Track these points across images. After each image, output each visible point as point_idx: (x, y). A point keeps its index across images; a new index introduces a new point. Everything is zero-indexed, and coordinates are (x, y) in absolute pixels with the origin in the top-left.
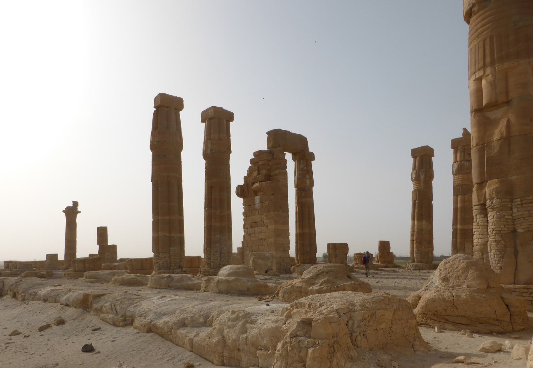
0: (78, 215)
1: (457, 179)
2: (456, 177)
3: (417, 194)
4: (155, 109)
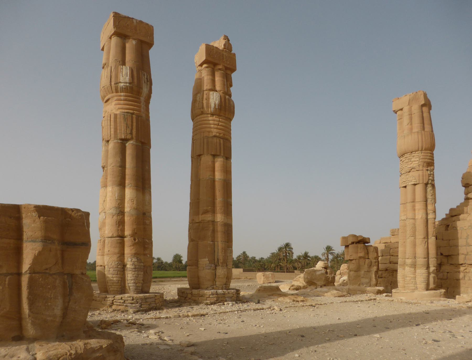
3: (132, 122)
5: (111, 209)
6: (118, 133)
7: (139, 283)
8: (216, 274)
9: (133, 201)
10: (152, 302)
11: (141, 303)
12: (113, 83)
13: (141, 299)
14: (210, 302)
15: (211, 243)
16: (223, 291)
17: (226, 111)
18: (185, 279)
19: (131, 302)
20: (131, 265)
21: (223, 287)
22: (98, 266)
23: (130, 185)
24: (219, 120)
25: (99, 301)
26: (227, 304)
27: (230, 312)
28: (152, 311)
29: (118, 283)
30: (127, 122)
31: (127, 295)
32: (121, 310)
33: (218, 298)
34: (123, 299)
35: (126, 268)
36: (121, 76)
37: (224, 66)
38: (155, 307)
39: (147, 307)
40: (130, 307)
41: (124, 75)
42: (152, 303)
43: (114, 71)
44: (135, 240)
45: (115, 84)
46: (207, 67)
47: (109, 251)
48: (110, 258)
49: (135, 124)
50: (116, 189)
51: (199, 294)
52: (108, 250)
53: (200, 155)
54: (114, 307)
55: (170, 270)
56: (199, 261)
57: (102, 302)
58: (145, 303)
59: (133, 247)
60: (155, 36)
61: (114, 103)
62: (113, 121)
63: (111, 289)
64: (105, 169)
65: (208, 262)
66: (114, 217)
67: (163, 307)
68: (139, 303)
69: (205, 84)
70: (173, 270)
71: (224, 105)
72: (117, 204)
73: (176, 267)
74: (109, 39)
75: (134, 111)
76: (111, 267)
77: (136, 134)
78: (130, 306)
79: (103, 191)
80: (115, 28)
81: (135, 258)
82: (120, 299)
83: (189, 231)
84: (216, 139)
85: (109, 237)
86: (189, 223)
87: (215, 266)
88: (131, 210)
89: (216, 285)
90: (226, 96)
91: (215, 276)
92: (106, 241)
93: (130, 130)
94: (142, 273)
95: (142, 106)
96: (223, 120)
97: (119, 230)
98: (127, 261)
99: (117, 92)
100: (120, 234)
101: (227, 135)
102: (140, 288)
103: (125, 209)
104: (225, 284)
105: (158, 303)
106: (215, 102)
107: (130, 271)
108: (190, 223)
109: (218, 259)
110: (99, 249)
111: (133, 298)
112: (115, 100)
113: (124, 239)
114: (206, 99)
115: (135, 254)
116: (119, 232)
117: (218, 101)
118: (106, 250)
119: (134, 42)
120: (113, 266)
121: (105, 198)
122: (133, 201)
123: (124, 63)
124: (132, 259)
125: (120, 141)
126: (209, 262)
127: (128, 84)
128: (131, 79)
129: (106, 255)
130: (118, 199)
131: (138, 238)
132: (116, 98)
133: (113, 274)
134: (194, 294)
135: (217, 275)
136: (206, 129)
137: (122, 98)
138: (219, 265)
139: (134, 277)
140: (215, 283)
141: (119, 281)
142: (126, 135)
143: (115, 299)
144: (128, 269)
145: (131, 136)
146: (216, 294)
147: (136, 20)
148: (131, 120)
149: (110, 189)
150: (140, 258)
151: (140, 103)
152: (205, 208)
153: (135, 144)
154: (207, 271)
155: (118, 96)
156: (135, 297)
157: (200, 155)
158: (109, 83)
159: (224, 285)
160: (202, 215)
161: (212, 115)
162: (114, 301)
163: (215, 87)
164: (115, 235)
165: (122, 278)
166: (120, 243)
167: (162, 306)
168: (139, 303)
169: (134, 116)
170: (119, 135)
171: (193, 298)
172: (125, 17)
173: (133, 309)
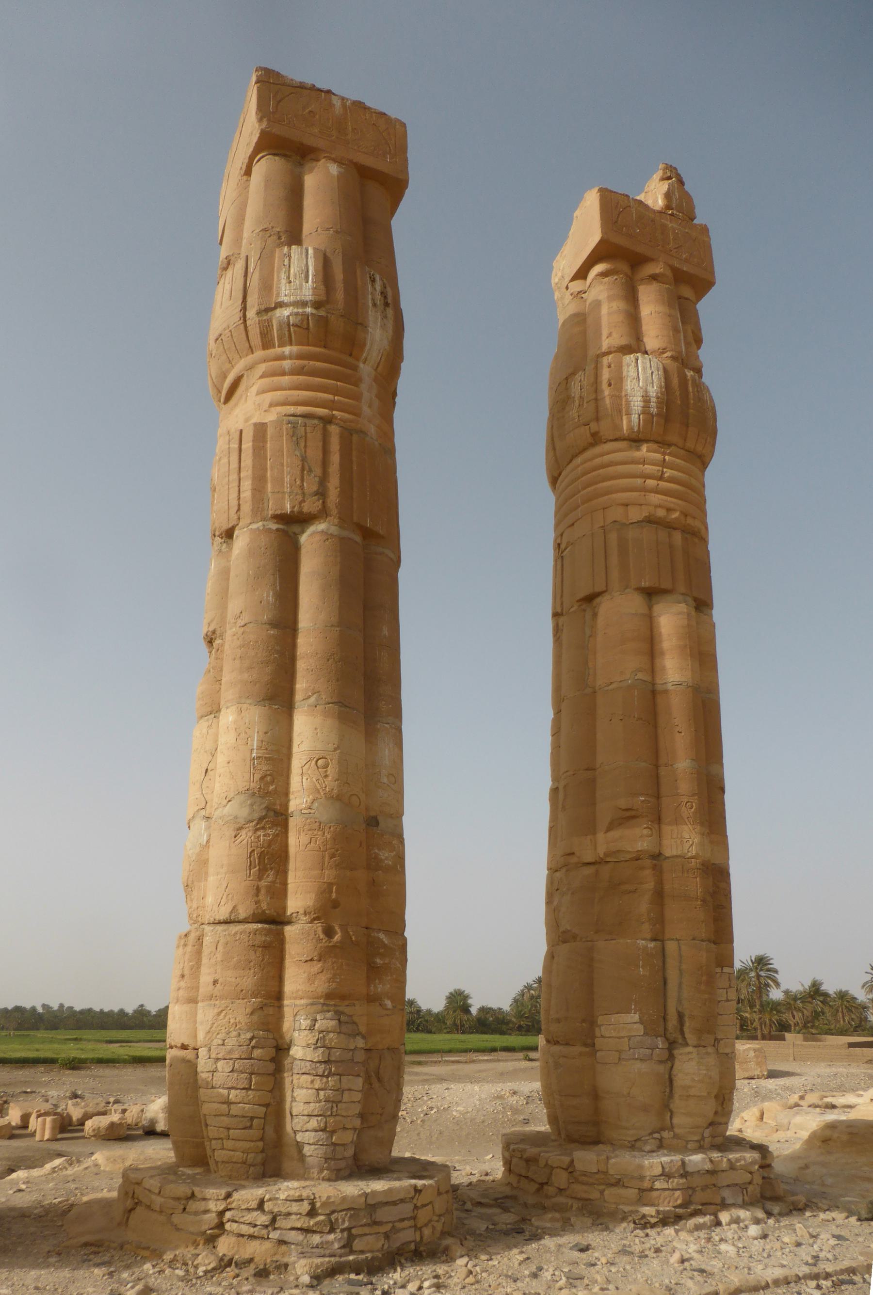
3: (326, 451)
4: (40, 1010)
5: (229, 801)
6: (270, 495)
7: (345, 1128)
8: (671, 1081)
9: (326, 766)
10: (402, 1220)
11: (349, 1229)
12: (251, 314)
13: (353, 1209)
14: (658, 1212)
15: (652, 945)
16: (711, 1161)
17: (687, 426)
18: (481, 1058)
19: (305, 1226)
20: (308, 1045)
21: (703, 1138)
22: (171, 1047)
23: (312, 700)
24: (664, 460)
25: (161, 1212)
26: (729, 1224)
27: (777, 1283)
28: (399, 1269)
29: (251, 1127)
30: (305, 451)
31: (289, 1189)
32: (256, 1260)
33: (690, 1192)
34: (267, 1206)
35: (286, 1062)
36: (284, 281)
37: (669, 266)
38: (413, 1247)
39: (380, 1245)
40: (300, 1249)
41: (295, 275)
42: (399, 1225)
43: (258, 268)
44: (329, 932)
45: (259, 313)
46: (603, 274)
47: (215, 982)
48: (219, 1014)
49: (335, 459)
50: (255, 714)
51: (606, 1173)
52: (210, 980)
53: (590, 598)
54: (225, 1246)
55: (440, 1031)
56: (599, 1023)
57: (177, 1219)
58: (366, 1230)
59: (320, 965)
60: (411, 154)
61: (254, 390)
62: (250, 451)
63: (220, 1155)
64: (217, 642)
65: (641, 1027)
66: (243, 832)
67: (449, 1241)
68: (342, 1231)
69: (605, 332)
70: (448, 1033)
71: (679, 402)
72: (257, 777)
73: (455, 1024)
74: (245, 178)
75: (332, 409)
76: (220, 1056)
77: (339, 496)
78: (297, 1244)
79: (205, 731)
80: (265, 120)
81: (329, 1015)
82: (253, 1209)
83: (549, 901)
84: (656, 528)
85: (220, 923)
86: (549, 869)
87: (667, 1045)
88: (316, 805)
89: (672, 1128)
90: (686, 370)
91: (668, 1090)
92: (207, 940)
93: (317, 479)
94: (359, 1083)
95: (366, 395)
96: (678, 461)
97: (263, 891)
98: (294, 1030)
99: (267, 344)
100: (264, 906)
101: (694, 518)
102: (350, 1152)
103: (289, 801)
104: (711, 1124)
105: (426, 1225)
106: (646, 391)
107: (305, 1076)
108: (553, 870)
109: (681, 1016)
110: (180, 973)
111: (312, 1204)
112: (261, 377)
113: (283, 929)
114: (610, 385)
115: (329, 996)
116: (261, 897)
117: (655, 388)
118: (206, 978)
119: (334, 169)
120: (231, 1052)
121: (210, 758)
122: (326, 766)
123: (294, 236)
124: (316, 1020)
125: (274, 526)
126: (645, 1027)
127: (309, 310)
128: (322, 287)
129: (203, 1001)
130: (259, 758)
131: (341, 926)
132: (262, 368)
133: (233, 1088)
134: (584, 1174)
135: (675, 1084)
136: (614, 496)
137: (287, 364)
138: (684, 1038)
139: (320, 1101)
140: (668, 1118)
141: (255, 1120)
142: (300, 498)
143: (233, 1205)
144: (297, 1062)
145: (321, 501)
146: (682, 1176)
147: (343, 99)
148: (321, 444)
149: (231, 718)
150: (351, 1016)
151: (357, 383)
152: (623, 803)
153: (336, 533)
154: (638, 1066)
155: (271, 360)
156: (324, 1199)
157: (590, 598)
158: (238, 315)
159: (707, 1128)
160: (609, 829)
161: (634, 444)
162: (228, 1215)
163: (642, 341)
164: (242, 914)
165: (267, 1105)
166: (266, 947)
167: (444, 1234)
168: (342, 1231)
169: (334, 429)
170: (271, 503)
171: (579, 1189)
172: (302, 86)
173: (310, 1260)
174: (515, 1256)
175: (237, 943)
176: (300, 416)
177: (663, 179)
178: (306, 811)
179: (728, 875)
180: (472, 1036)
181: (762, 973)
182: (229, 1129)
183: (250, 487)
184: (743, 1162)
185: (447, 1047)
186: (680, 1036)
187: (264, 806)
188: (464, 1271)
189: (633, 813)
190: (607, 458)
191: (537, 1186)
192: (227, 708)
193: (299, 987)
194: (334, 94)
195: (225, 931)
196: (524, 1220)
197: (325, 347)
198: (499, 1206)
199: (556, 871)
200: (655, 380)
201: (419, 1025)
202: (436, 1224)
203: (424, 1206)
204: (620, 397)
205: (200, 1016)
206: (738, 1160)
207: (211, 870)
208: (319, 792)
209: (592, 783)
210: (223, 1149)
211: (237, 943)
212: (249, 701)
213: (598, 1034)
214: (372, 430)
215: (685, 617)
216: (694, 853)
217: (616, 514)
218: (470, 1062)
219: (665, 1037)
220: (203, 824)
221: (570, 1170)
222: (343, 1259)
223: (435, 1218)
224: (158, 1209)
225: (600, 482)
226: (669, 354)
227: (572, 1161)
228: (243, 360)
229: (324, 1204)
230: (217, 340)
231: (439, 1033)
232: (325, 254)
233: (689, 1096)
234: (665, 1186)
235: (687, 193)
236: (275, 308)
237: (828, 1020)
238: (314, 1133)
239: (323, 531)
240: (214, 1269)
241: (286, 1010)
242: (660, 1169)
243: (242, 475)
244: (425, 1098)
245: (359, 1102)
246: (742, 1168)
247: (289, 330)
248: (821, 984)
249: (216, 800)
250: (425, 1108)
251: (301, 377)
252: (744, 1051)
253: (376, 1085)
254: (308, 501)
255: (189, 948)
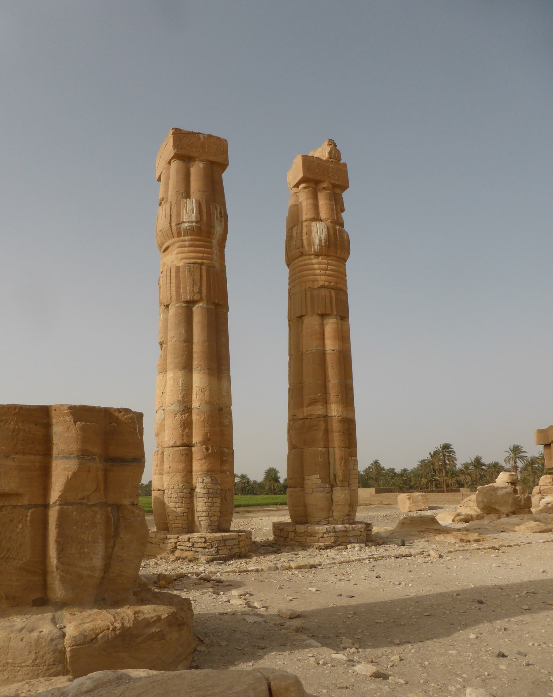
0: (386, 465)
1: (321, 269)
2: (320, 263)
3: (201, 276)
6: (182, 293)
7: (215, 516)
8: (332, 499)
9: (205, 392)
10: (235, 545)
11: (217, 547)
12: (173, 224)
14: (325, 545)
15: (324, 450)
20: (202, 488)
21: (344, 520)
22: (154, 490)
23: (199, 368)
24: (328, 262)
25: (156, 544)
27: (356, 560)
28: (234, 560)
29: (183, 516)
31: (197, 535)
33: (337, 538)
35: (194, 494)
36: (185, 213)
38: (238, 554)
39: (227, 553)
40: (202, 553)
43: (175, 207)
44: (207, 449)
45: (176, 225)
46: (305, 188)
47: (170, 467)
48: (172, 478)
49: (204, 278)
50: (180, 374)
51: (307, 532)
53: (301, 317)
54: (177, 553)
55: (261, 493)
56: (305, 479)
58: (223, 548)
59: (205, 460)
61: (175, 252)
63: (173, 525)
69: (304, 213)
70: (266, 494)
71: (333, 240)
72: (181, 396)
73: (270, 489)
76: (172, 492)
79: (161, 378)
80: (176, 149)
82: (187, 541)
83: (288, 433)
84: (325, 290)
86: (288, 420)
87: (330, 486)
88: (201, 405)
89: (333, 516)
91: (331, 503)
92: (166, 453)
93: (198, 287)
97: (185, 436)
99: (179, 235)
100: (185, 441)
102: (216, 524)
103: (192, 404)
104: (348, 515)
106: (320, 237)
108: (290, 421)
109: (335, 476)
111: (205, 539)
114: (307, 234)
115: (208, 471)
116: (184, 438)
118: (166, 466)
119: (201, 165)
120: (176, 491)
122: (205, 392)
123: (187, 195)
125: (184, 305)
127: (194, 224)
128: (199, 215)
129: (165, 474)
132: (178, 244)
134: (300, 533)
135: (333, 501)
136: (309, 277)
137: (187, 243)
138: (337, 484)
139: (206, 506)
143: (180, 540)
145: (200, 295)
146: (334, 532)
148: (199, 273)
152: (312, 396)
157: (301, 317)
158: (169, 225)
159: (346, 516)
160: (307, 407)
162: (178, 543)
164: (178, 444)
165: (188, 508)
166: (186, 455)
167: (249, 551)
168: (215, 548)
169: (204, 267)
170: (182, 297)
171: (298, 539)
172: (189, 133)
174: (273, 556)
175: (177, 454)
176: (192, 263)
177: (328, 145)
178: (198, 408)
179: (355, 422)
180: (280, 495)
181: (447, 454)
182: (176, 516)
183: (175, 290)
184: (357, 528)
185: (265, 502)
186: (335, 483)
187: (184, 406)
188: (255, 560)
189: (316, 400)
190: (306, 262)
191: (284, 539)
192: (170, 371)
193: (198, 468)
194: (200, 133)
195: (172, 450)
196: (279, 550)
197: (200, 236)
198: (270, 546)
199: (291, 421)
200: (324, 233)
201: (249, 490)
202: (246, 548)
203: (242, 541)
204: (311, 239)
205: (164, 479)
206: (356, 527)
207: (166, 429)
208: (202, 401)
209: (302, 388)
210: (175, 523)
211: (177, 454)
212: (178, 369)
213: (305, 483)
214: (217, 265)
215: (336, 324)
216: (339, 415)
217: (309, 285)
218: (278, 510)
219: (329, 483)
220: (162, 412)
221: (295, 532)
222: (216, 556)
223: (246, 546)
224: (155, 543)
225: (304, 271)
226: (329, 221)
227: (295, 529)
228: (170, 240)
229: (209, 539)
230: (160, 231)
231: (261, 495)
232: (199, 202)
233: (338, 505)
234: (328, 536)
235: (338, 151)
236: (182, 223)
237: (487, 480)
238: (204, 517)
239: (201, 307)
240: (175, 560)
241: (194, 476)
242: (326, 530)
243: (172, 285)
244: (249, 524)
245: (219, 507)
246: (357, 529)
247: (187, 231)
248: (481, 458)
249: (167, 404)
250: (249, 529)
251: (192, 248)
252: (416, 496)
253: (225, 501)
254: (195, 295)
255: (159, 456)
